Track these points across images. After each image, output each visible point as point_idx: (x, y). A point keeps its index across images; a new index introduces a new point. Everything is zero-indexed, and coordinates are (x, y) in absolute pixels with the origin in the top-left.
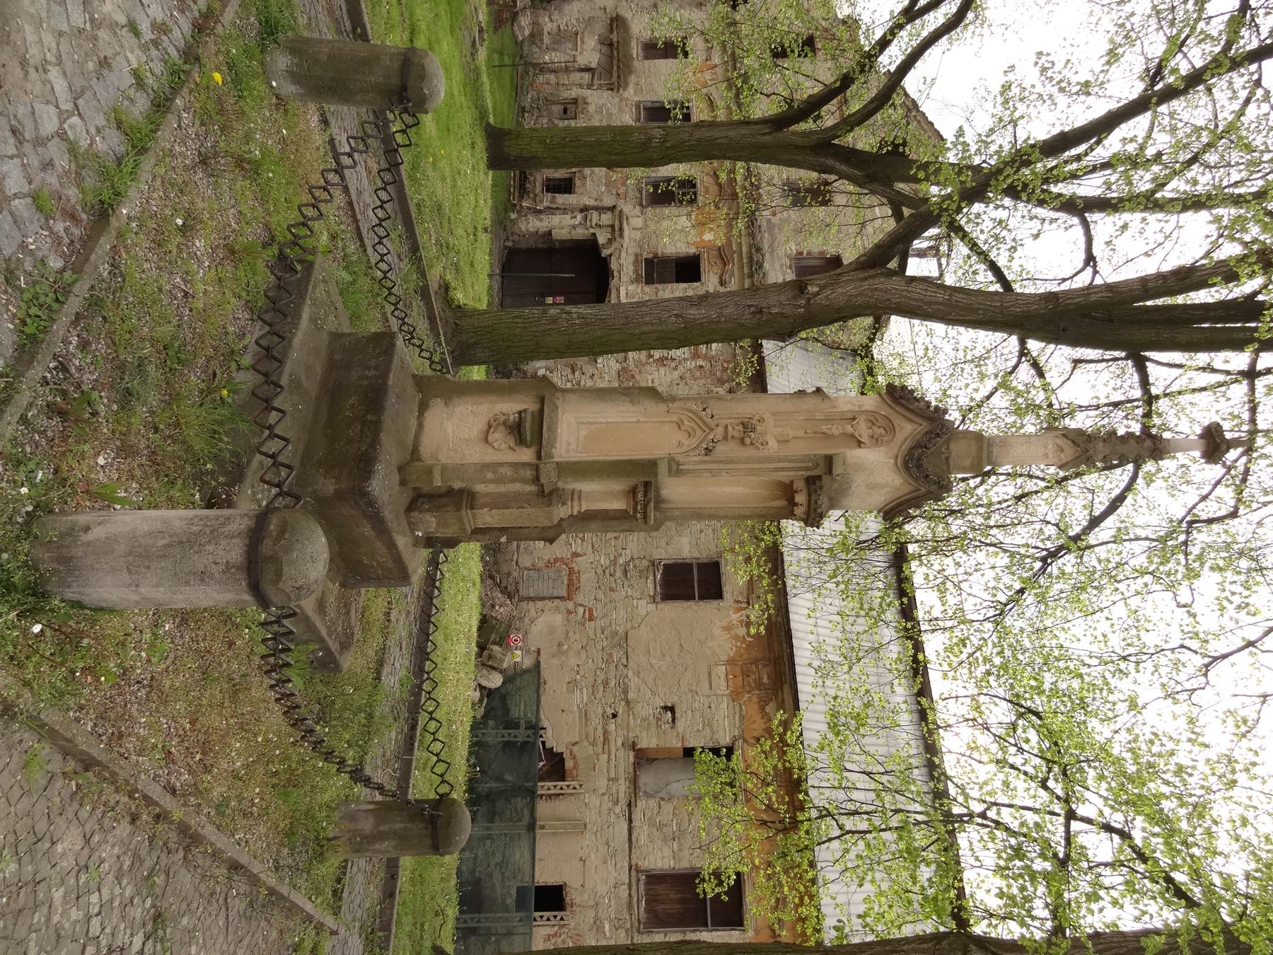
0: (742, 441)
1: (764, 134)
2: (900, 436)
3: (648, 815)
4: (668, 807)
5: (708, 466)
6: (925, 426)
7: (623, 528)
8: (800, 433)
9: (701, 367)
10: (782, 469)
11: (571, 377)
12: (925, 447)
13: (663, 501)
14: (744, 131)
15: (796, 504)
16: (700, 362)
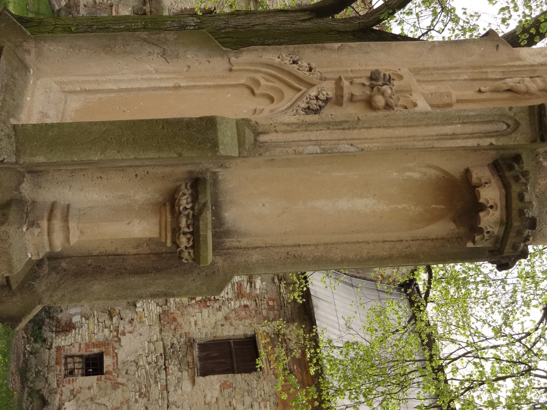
1: (304, 21)
7: (152, 289)
9: (246, 306)
10: (454, 136)
11: (108, 323)
13: (227, 233)
14: (282, 19)
15: (482, 207)
16: (245, 302)
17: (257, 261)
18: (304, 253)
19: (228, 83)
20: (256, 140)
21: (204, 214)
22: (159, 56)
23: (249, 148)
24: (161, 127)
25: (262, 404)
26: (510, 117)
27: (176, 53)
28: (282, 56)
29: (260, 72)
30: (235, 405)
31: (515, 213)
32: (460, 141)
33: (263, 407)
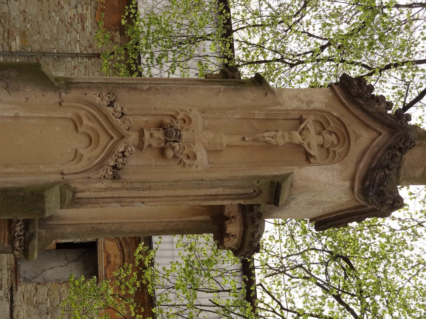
0: (162, 152)
2: (356, 148)
3: (27, 296)
4: (43, 290)
5: (116, 194)
6: (384, 137)
8: (236, 140)
12: (387, 167)
17: (71, 232)
18: (104, 228)
19: (58, 116)
20: (74, 196)
21: (32, 242)
22: (3, 89)
23: (68, 204)
24: (2, 199)
25: (85, 7)
26: (257, 187)
27: (17, 87)
28: (102, 95)
29: (84, 109)
30: (62, 5)
31: (246, 244)
32: (219, 201)
33: (85, 9)
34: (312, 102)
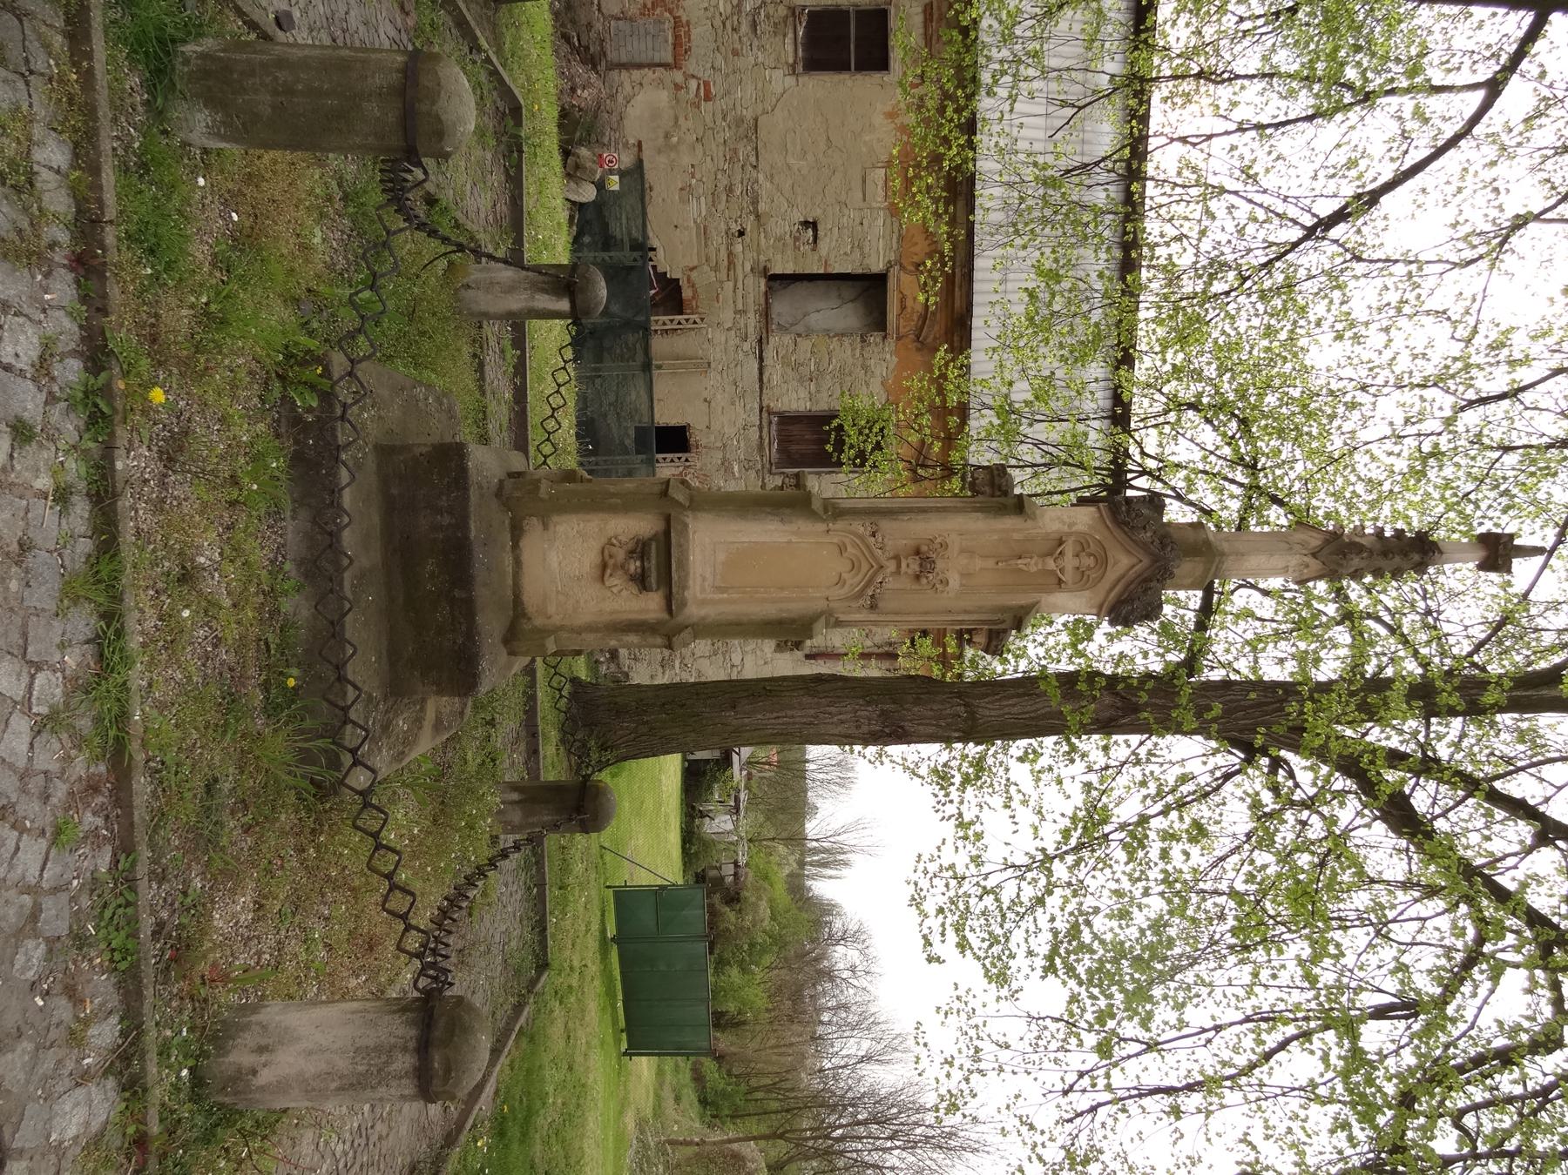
4: (805, 345)
34: (1074, 524)
